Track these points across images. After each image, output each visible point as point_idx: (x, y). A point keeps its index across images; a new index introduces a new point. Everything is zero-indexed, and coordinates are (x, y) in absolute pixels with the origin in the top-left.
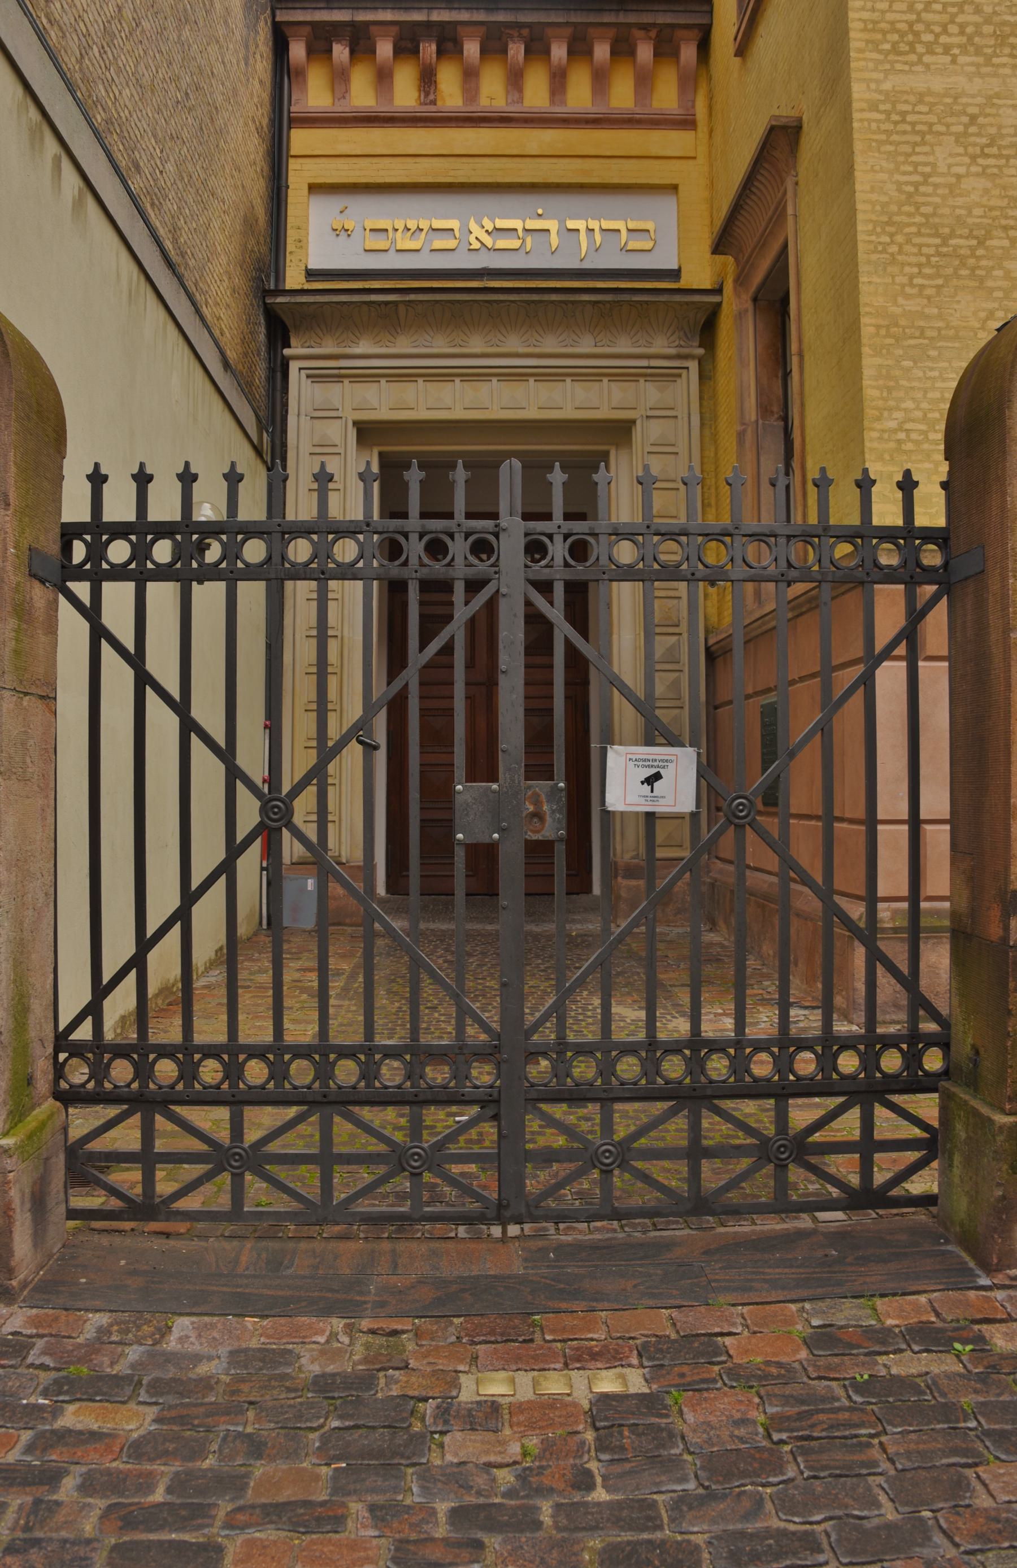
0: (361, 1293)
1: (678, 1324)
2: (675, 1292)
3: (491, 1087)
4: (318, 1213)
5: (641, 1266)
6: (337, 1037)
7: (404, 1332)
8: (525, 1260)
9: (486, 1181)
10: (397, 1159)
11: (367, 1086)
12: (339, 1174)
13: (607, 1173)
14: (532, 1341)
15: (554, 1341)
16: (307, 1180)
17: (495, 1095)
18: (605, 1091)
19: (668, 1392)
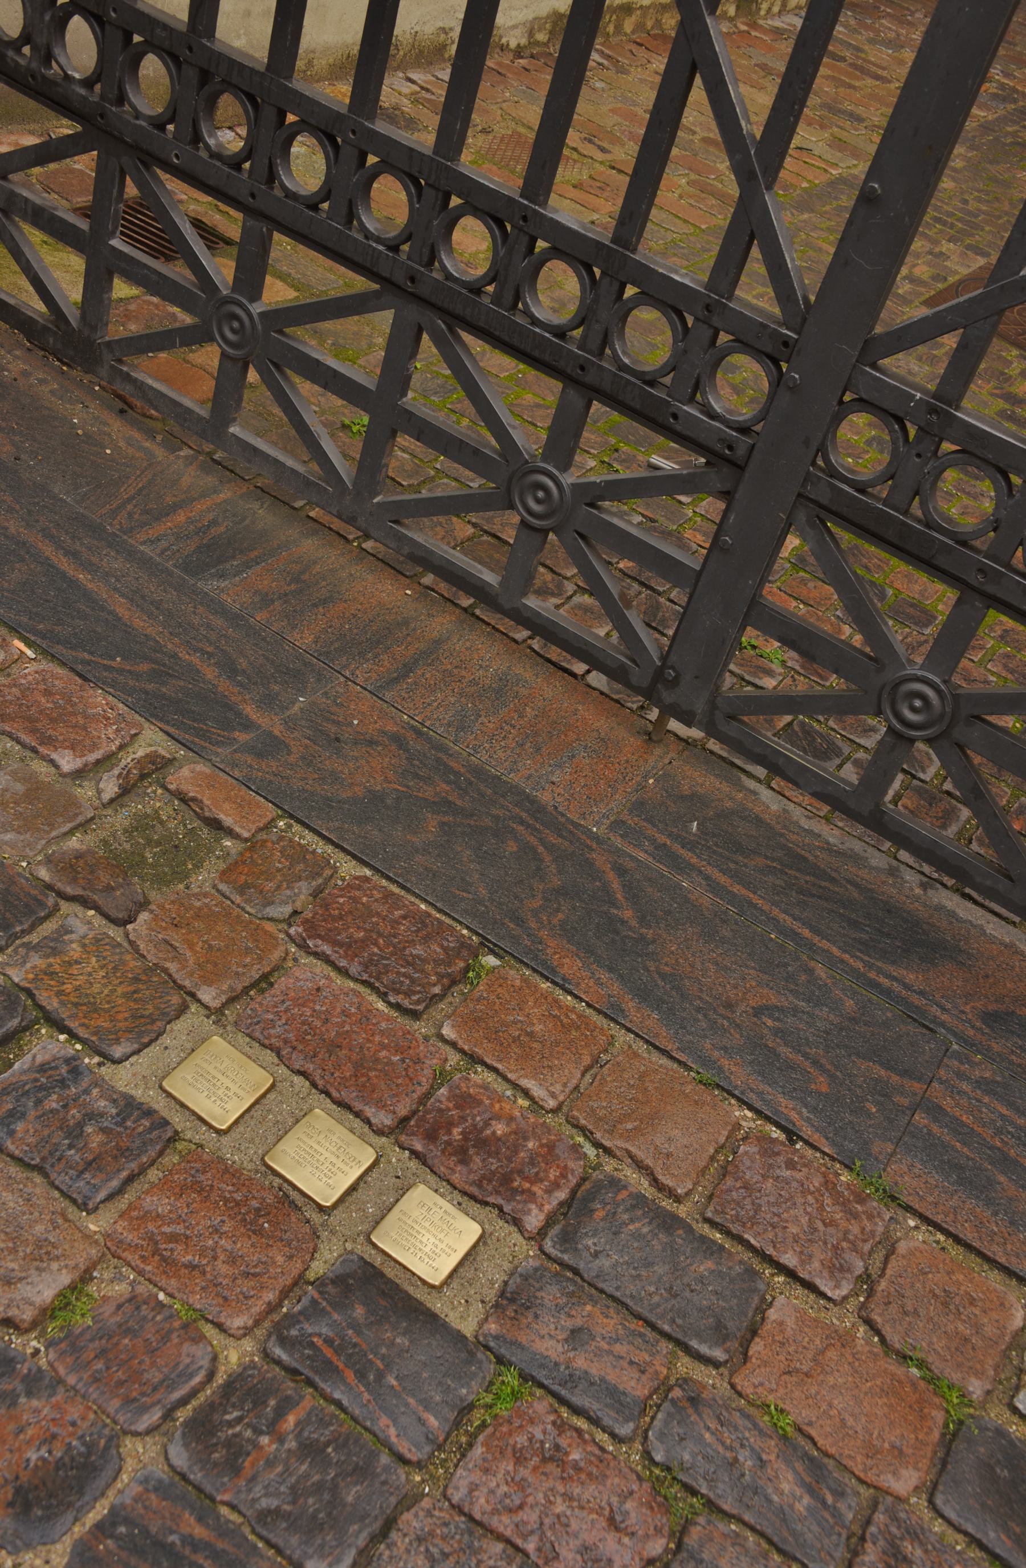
0: (268, 702)
1: (729, 1182)
2: (821, 1083)
3: (744, 430)
4: (360, 508)
5: (831, 962)
6: (470, 161)
7: (230, 833)
8: (639, 807)
9: (795, 582)
10: (509, 476)
11: (497, 299)
12: (405, 452)
13: (899, 739)
14: (415, 1015)
15: (453, 1044)
16: (337, 429)
17: (741, 451)
18: (982, 570)
19: (500, 1360)
